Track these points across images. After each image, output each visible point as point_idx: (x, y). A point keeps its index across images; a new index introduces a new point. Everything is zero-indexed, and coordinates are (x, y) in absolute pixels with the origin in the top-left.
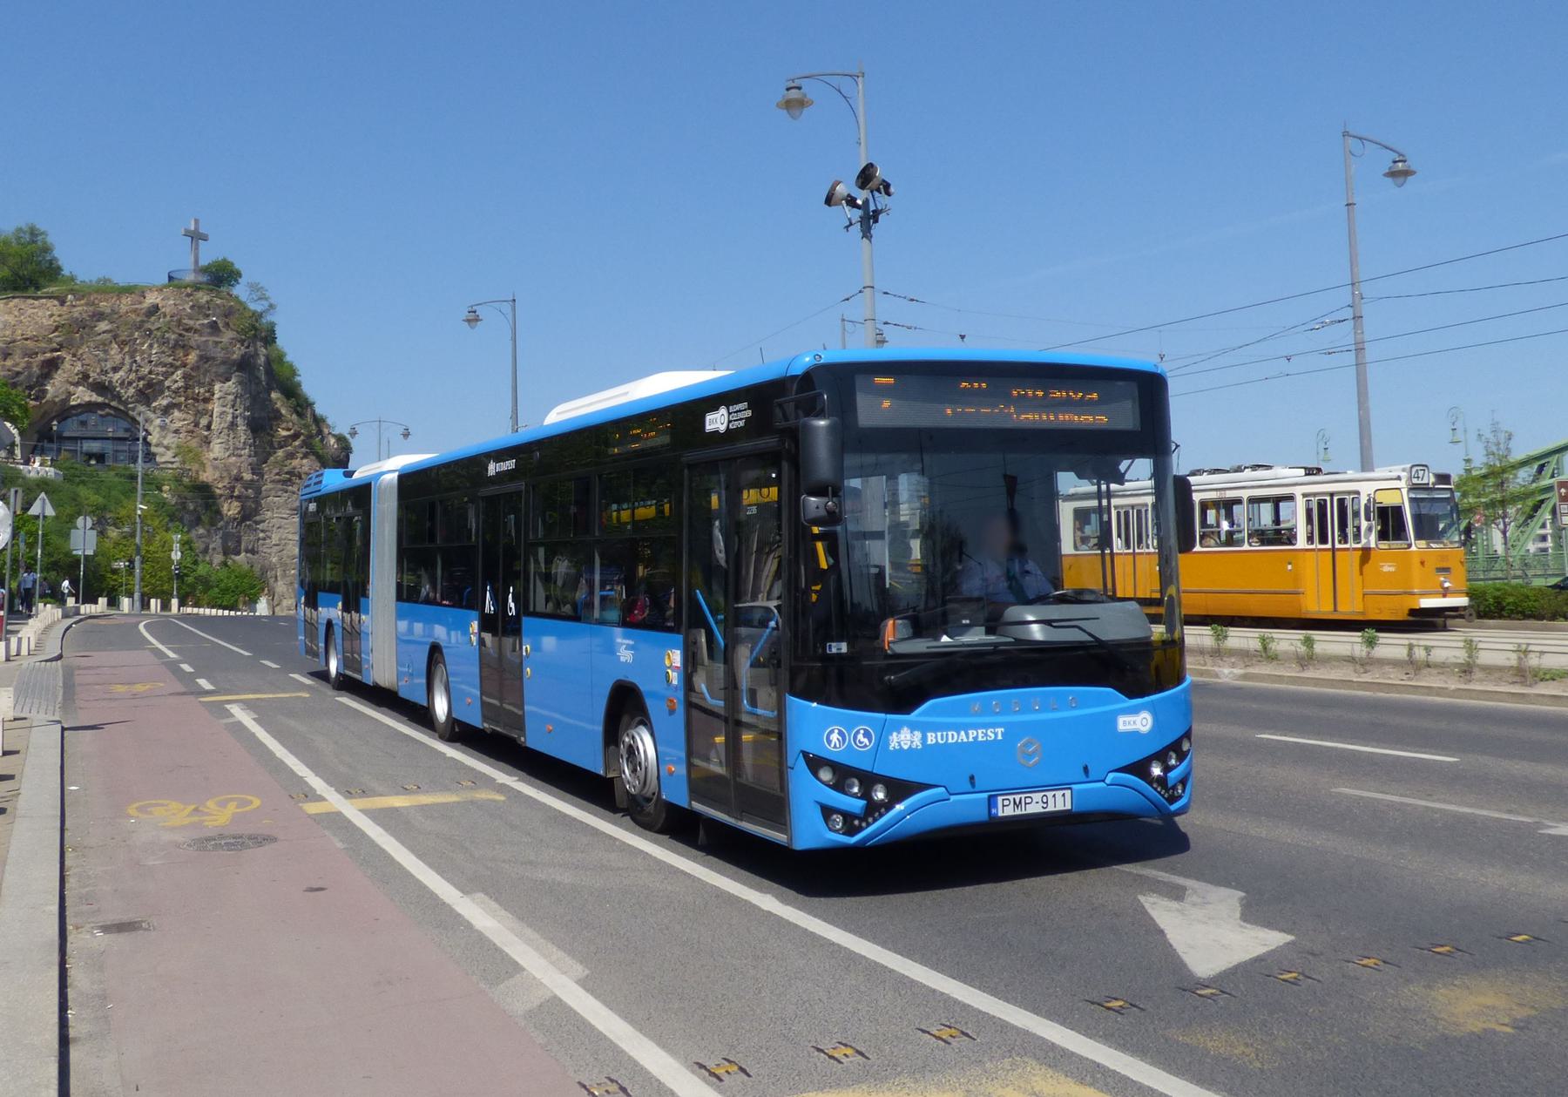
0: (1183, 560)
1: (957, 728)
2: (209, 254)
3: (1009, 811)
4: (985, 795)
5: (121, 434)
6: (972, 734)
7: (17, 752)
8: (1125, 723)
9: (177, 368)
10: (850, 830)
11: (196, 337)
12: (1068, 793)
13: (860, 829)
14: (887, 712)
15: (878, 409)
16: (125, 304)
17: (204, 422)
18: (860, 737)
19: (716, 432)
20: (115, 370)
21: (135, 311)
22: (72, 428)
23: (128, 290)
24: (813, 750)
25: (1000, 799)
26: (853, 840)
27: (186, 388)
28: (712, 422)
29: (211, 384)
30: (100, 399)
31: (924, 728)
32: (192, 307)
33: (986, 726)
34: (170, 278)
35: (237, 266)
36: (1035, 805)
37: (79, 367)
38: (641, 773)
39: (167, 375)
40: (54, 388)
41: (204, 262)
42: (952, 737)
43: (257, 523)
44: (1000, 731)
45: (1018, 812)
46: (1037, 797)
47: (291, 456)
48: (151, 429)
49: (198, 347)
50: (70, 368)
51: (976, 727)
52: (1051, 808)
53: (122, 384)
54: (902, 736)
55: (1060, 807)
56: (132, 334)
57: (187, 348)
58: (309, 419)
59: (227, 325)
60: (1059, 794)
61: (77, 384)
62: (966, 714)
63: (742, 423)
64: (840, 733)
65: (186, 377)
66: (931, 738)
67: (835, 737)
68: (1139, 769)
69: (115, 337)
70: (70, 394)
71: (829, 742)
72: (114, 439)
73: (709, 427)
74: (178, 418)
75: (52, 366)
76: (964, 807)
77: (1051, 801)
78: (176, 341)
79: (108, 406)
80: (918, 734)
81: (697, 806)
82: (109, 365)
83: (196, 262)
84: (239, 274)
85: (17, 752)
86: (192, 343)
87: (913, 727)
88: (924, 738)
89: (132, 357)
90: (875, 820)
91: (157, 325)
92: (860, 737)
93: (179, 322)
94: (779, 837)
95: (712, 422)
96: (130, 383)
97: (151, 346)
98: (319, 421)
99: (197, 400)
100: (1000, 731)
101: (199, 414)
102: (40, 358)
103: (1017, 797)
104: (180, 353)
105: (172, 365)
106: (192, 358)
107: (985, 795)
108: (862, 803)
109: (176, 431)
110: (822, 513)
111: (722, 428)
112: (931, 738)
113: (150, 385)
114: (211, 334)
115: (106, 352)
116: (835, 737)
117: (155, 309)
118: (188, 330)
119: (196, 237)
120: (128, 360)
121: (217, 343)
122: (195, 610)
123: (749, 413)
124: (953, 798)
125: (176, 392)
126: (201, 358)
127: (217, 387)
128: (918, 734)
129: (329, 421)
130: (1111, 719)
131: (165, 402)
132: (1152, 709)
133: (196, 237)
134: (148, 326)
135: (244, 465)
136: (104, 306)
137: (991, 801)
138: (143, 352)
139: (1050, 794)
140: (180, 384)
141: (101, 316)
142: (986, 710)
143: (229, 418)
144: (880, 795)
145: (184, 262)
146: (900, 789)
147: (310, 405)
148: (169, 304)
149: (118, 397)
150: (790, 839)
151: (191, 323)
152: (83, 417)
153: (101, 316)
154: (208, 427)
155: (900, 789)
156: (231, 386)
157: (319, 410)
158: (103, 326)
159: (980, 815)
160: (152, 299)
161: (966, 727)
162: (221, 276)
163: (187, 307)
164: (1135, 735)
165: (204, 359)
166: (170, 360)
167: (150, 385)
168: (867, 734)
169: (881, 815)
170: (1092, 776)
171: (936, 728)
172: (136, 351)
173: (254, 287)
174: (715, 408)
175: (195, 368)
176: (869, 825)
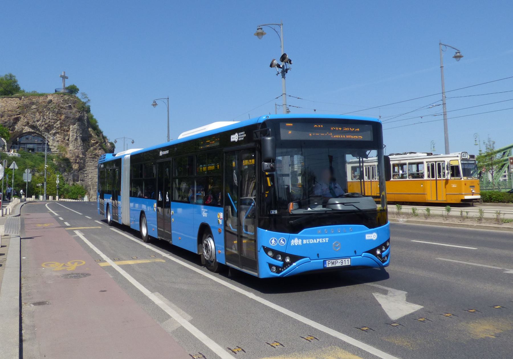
0: (387, 183)
1: (313, 238)
2: (68, 83)
3: (330, 265)
4: (322, 260)
5: (40, 142)
6: (318, 240)
7: (6, 246)
8: (368, 237)
9: (58, 120)
10: (278, 272)
11: (64, 110)
12: (349, 259)
13: (281, 271)
14: (290, 233)
15: (287, 134)
16: (41, 99)
17: (67, 138)
18: (281, 241)
19: (234, 141)
20: (38, 121)
21: (44, 102)
22: (23, 140)
23: (42, 95)
24: (266, 245)
25: (327, 261)
26: (279, 275)
27: (61, 127)
28: (233, 138)
29: (69, 126)
30: (33, 131)
31: (302, 238)
32: (63, 101)
33: (323, 238)
34: (56, 91)
35: (78, 87)
36: (339, 263)
37: (26, 120)
38: (210, 253)
39: (55, 123)
40: (18, 127)
41: (67, 86)
42: (312, 241)
43: (84, 171)
44: (327, 239)
45: (333, 266)
46: (339, 261)
47: (95, 149)
48: (49, 140)
49: (65, 114)
50: (23, 120)
51: (319, 238)
52: (344, 264)
53: (40, 126)
54: (295, 241)
55: (347, 264)
56: (43, 109)
57: (61, 114)
58: (101, 137)
59: (74, 106)
60: (346, 260)
61: (25, 126)
62: (316, 234)
63: (243, 139)
64: (275, 240)
65: (61, 123)
66: (305, 242)
67: (273, 241)
68: (373, 252)
69: (38, 110)
70: (23, 129)
71: (271, 243)
72: (37, 144)
73: (232, 140)
74: (58, 137)
75: (17, 120)
76: (315, 264)
77: (344, 262)
78: (58, 112)
79: (35, 133)
80: (300, 240)
81: (228, 264)
82: (36, 119)
83: (64, 86)
84: (78, 90)
85: (6, 246)
86: (63, 112)
87: (299, 238)
88: (302, 242)
89: (43, 117)
90: (286, 268)
91: (51, 106)
92: (281, 241)
93: (59, 105)
94: (255, 274)
95: (233, 138)
96: (43, 125)
97: (49, 113)
98: (104, 138)
99: (64, 131)
100: (327, 239)
101: (65, 135)
102: (13, 117)
103: (333, 261)
104: (59, 116)
105: (56, 120)
106: (63, 117)
107: (322, 260)
108: (282, 263)
109: (58, 141)
110: (269, 168)
111: (236, 140)
112: (305, 242)
113: (49, 126)
114: (69, 109)
115: (35, 115)
116: (273, 241)
117: (51, 101)
118: (62, 108)
119: (64, 77)
120: (42, 118)
121: (71, 112)
122: (64, 200)
123: (245, 135)
124: (312, 261)
125: (58, 128)
126: (66, 117)
127: (71, 127)
128: (300, 240)
129: (108, 138)
130: (364, 235)
131: (54, 132)
132: (377, 232)
133: (64, 77)
134: (48, 107)
135: (80, 152)
136: (34, 100)
137: (324, 262)
138: (47, 115)
139: (343, 260)
140: (59, 126)
141: (33, 103)
142: (323, 232)
143: (75, 137)
144: (288, 260)
145: (60, 86)
146: (294, 258)
147: (102, 133)
148: (55, 99)
149: (39, 130)
150: (259, 274)
151: (63, 106)
152: (27, 137)
153: (33, 103)
154: (68, 140)
155: (294, 258)
156: (76, 126)
157: (105, 134)
158: (34, 107)
159: (321, 267)
160: (50, 98)
161: (316, 238)
162: (72, 90)
163: (61, 101)
164: (371, 240)
165: (67, 117)
166: (56, 118)
167: (49, 126)
168: (284, 240)
169: (288, 267)
170: (357, 254)
171: (306, 238)
172: (44, 115)
173: (83, 94)
174: (234, 134)
175: (64, 120)
176: (284, 270)
